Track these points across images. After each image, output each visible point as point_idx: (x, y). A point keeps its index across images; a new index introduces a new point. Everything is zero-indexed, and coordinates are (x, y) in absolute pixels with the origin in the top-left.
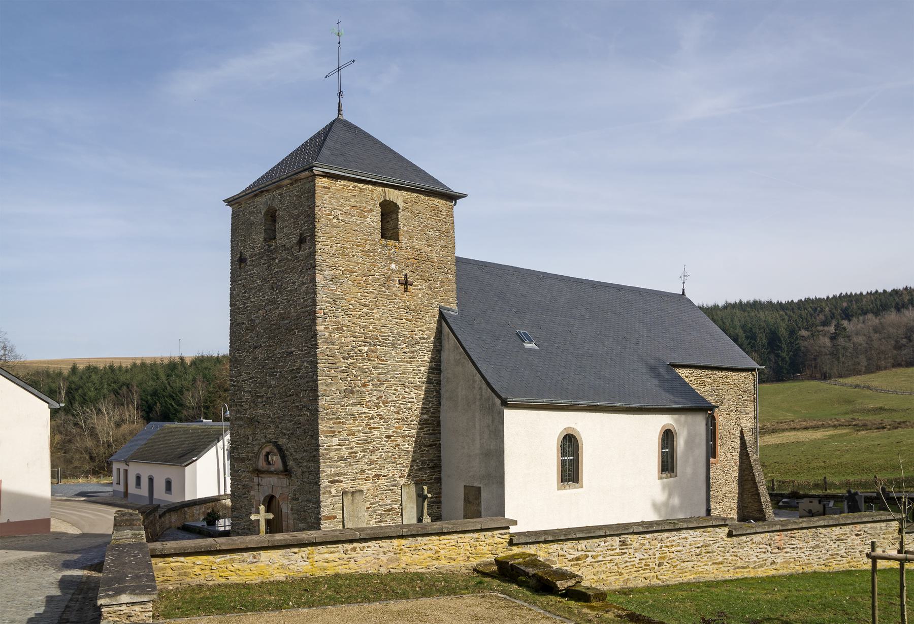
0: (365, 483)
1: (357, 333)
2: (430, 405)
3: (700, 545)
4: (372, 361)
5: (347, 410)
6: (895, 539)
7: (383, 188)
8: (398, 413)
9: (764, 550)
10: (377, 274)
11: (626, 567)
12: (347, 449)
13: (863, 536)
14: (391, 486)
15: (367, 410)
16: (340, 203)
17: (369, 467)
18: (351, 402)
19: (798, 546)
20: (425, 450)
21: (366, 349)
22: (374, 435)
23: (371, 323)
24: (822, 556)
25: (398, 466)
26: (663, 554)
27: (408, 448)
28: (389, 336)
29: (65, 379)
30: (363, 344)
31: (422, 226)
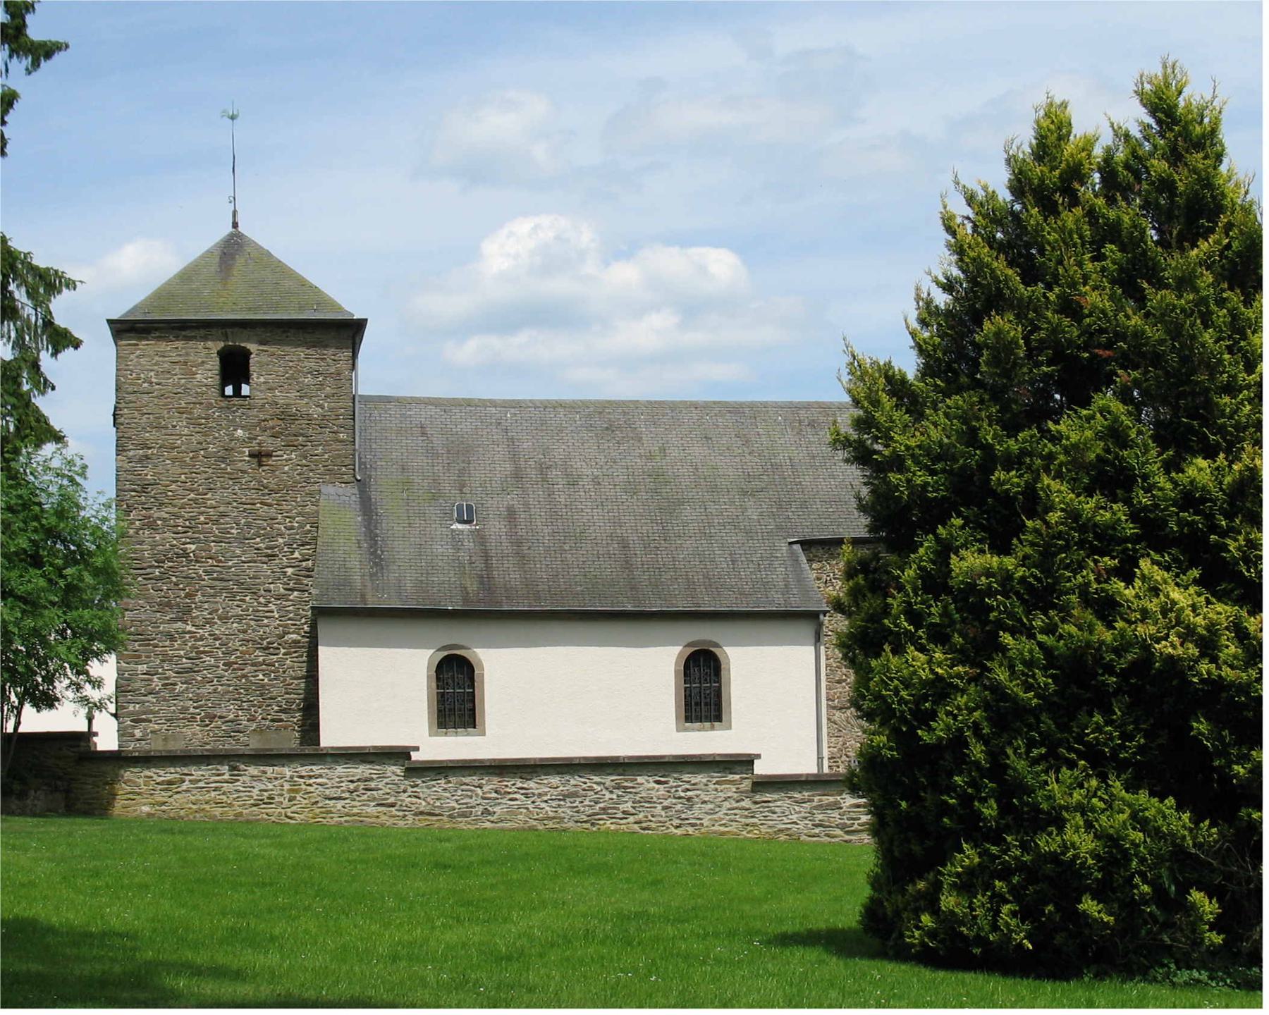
0: (188, 725)
1: (180, 528)
2: (303, 620)
3: (355, 779)
4: (203, 562)
5: (161, 628)
6: (741, 792)
7: (224, 330)
8: (245, 632)
9: (470, 793)
10: (212, 446)
11: (238, 797)
12: (159, 678)
13: (671, 784)
14: (233, 732)
15: (193, 629)
16: (154, 362)
17: (195, 704)
18: (168, 618)
19: (536, 792)
20: (292, 683)
21: (193, 547)
22: (205, 661)
23: (202, 513)
24: (582, 809)
25: (244, 704)
26: (294, 785)
27: (263, 680)
28: (232, 528)
29: (966, 644)
30: (188, 540)
31: (291, 372)
